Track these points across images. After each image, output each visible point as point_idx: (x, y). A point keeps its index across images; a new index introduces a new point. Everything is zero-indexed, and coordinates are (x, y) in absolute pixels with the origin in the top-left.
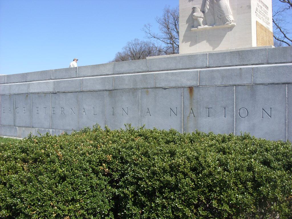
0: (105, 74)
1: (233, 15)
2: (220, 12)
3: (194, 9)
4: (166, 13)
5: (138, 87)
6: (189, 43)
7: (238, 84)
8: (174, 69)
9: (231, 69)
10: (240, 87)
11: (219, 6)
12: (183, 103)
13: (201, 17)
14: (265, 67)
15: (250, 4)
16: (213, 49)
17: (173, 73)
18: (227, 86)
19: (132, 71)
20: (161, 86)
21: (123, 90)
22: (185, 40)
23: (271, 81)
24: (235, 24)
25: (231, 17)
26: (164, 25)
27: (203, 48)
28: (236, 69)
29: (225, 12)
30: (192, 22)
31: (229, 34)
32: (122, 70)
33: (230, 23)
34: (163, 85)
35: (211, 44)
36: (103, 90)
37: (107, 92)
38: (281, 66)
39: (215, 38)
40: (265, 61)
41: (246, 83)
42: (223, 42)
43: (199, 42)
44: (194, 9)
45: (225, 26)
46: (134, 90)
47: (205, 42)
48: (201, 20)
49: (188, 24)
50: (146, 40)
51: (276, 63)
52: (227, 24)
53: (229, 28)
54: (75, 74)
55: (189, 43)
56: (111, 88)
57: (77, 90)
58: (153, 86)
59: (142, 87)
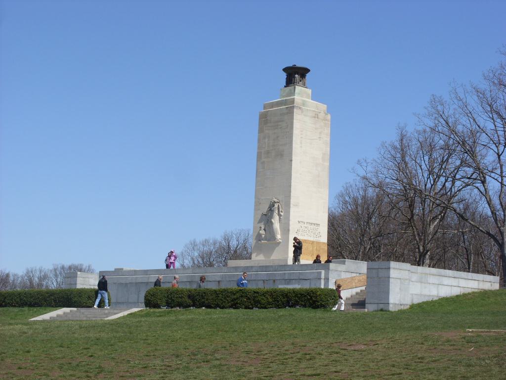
48: (263, 236)
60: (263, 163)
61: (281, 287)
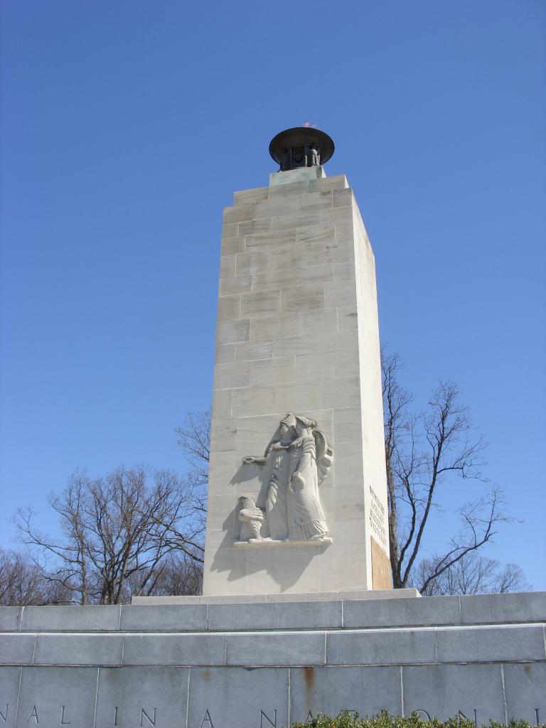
0: (98, 629)
1: (328, 522)
2: (302, 514)
3: (242, 502)
4: (74, 485)
5: (185, 662)
6: (229, 571)
7: (409, 661)
8: (268, 628)
9: (394, 634)
10: (412, 668)
11: (300, 501)
12: (292, 700)
13: (257, 520)
14: (459, 632)
15: (363, 501)
16: (283, 590)
17: (268, 637)
18: (385, 666)
19: (168, 628)
20: (240, 663)
21: (147, 669)
22: (219, 565)
23: (472, 657)
24: (332, 541)
25: (324, 526)
26: (69, 515)
27: (260, 586)
28: (404, 633)
29: (312, 514)
30: (237, 528)
31: (317, 559)
32: (145, 624)
33: (322, 538)
34: (246, 660)
35: (277, 579)
36: (94, 666)
37: (104, 672)
38: (489, 630)
39: (287, 568)
40: (458, 620)
41: (423, 660)
42: (303, 577)
43: (251, 572)
44: (242, 502)
45: (310, 542)
46: (174, 670)
47: (264, 572)
48: (258, 526)
49: (226, 532)
50: (21, 548)
51: (478, 624)
52: (316, 539)
53: (317, 547)
54: (14, 623)
55: (227, 573)
56: (115, 661)
57: (19, 662)
58: (221, 661)
59: (194, 663)
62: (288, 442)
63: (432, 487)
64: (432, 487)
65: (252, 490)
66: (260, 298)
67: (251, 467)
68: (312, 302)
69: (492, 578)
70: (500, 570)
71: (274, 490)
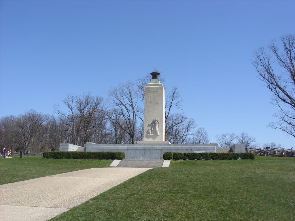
3: (148, 130)
11: (156, 130)
22: (146, 137)
25: (158, 133)
27: (150, 140)
30: (148, 133)
31: (158, 137)
39: (154, 138)
44: (148, 130)
47: (151, 138)
48: (151, 133)
60: (148, 106)
61: (195, 152)
62: (154, 122)
63: (170, 108)
64: (170, 108)
65: (150, 128)
66: (150, 102)
67: (149, 125)
68: (158, 103)
69: (185, 122)
70: (188, 120)
71: (153, 128)
